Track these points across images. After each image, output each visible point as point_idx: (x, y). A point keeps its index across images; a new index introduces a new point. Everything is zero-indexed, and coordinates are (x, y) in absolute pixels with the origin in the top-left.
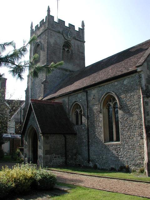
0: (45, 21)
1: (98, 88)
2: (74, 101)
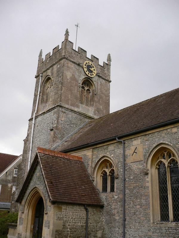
0: (60, 47)
1: (143, 137)
2: (101, 156)
